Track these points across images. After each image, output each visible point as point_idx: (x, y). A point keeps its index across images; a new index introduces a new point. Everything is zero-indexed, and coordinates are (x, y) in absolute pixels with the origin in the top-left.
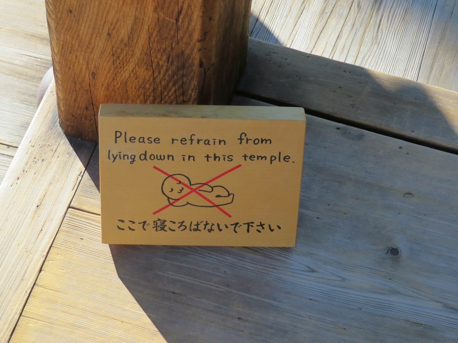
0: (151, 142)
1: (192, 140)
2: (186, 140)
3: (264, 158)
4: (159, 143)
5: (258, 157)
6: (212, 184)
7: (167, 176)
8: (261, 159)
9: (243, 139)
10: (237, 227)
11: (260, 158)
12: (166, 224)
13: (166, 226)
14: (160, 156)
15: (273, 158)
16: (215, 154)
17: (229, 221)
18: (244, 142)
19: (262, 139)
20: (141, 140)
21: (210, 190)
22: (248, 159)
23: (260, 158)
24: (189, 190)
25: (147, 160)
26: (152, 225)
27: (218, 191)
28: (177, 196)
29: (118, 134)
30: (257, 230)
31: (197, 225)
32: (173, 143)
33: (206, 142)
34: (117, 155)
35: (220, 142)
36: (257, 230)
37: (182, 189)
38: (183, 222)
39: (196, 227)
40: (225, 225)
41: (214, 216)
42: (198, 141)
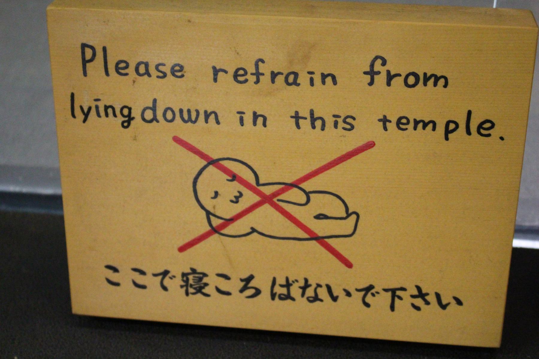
0: (165, 75)
1: (258, 74)
2: (246, 73)
3: (431, 125)
4: (182, 76)
5: (416, 123)
6: (307, 186)
7: (204, 163)
8: (424, 128)
9: (379, 73)
10: (369, 295)
11: (420, 125)
12: (205, 280)
13: (206, 285)
14: (189, 111)
15: (452, 126)
16: (312, 113)
17: (356, 279)
18: (380, 80)
19: (425, 74)
20: (142, 69)
21: (304, 200)
22: (391, 126)
23: (420, 125)
24: (256, 199)
25: (158, 121)
26: (179, 281)
27: (320, 204)
28: (227, 210)
29: (89, 53)
30: (414, 306)
31: (288, 285)
32: (215, 80)
33: (291, 79)
34: (90, 109)
35: (324, 77)
36: (414, 306)
37: (238, 194)
38: (251, 277)
39: (284, 291)
40: (345, 290)
41: (311, 263)
42: (274, 76)
